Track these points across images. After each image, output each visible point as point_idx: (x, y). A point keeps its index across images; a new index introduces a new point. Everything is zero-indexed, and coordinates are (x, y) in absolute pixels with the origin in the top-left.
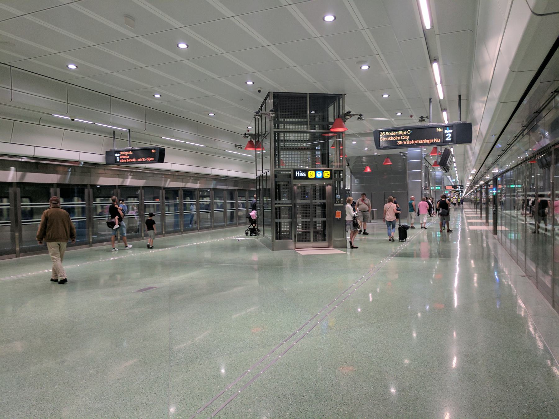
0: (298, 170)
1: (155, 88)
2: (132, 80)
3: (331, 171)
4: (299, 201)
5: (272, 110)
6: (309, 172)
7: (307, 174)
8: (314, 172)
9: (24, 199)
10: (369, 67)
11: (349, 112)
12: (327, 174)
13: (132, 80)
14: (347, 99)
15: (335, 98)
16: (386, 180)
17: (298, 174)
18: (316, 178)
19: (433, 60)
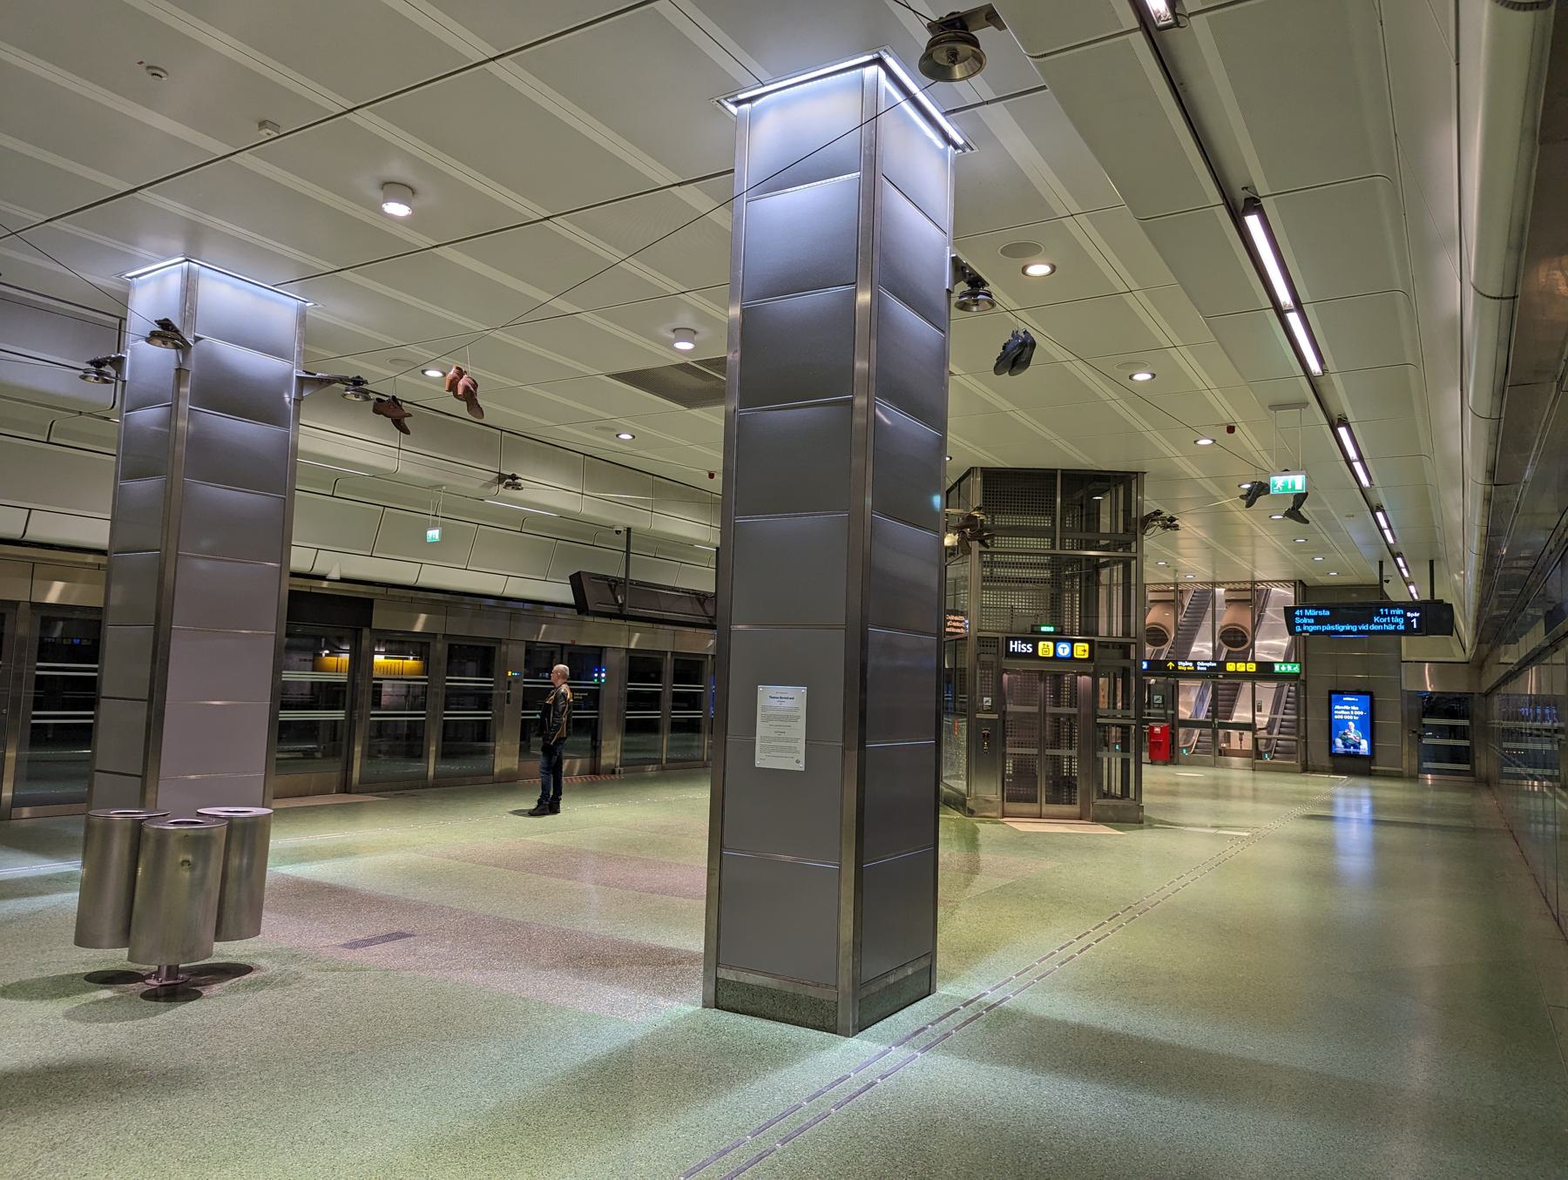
0: (1014, 639)
1: (623, 421)
2: (580, 406)
3: (1090, 642)
4: (1050, 710)
5: (979, 509)
6: (1041, 644)
7: (1035, 648)
8: (1051, 644)
9: (296, 658)
10: (1054, 268)
11: (1158, 513)
12: (1081, 650)
13: (580, 406)
14: (1148, 484)
15: (1124, 481)
16: (367, 392)
17: (1015, 646)
18: (1055, 658)
19: (1240, 206)
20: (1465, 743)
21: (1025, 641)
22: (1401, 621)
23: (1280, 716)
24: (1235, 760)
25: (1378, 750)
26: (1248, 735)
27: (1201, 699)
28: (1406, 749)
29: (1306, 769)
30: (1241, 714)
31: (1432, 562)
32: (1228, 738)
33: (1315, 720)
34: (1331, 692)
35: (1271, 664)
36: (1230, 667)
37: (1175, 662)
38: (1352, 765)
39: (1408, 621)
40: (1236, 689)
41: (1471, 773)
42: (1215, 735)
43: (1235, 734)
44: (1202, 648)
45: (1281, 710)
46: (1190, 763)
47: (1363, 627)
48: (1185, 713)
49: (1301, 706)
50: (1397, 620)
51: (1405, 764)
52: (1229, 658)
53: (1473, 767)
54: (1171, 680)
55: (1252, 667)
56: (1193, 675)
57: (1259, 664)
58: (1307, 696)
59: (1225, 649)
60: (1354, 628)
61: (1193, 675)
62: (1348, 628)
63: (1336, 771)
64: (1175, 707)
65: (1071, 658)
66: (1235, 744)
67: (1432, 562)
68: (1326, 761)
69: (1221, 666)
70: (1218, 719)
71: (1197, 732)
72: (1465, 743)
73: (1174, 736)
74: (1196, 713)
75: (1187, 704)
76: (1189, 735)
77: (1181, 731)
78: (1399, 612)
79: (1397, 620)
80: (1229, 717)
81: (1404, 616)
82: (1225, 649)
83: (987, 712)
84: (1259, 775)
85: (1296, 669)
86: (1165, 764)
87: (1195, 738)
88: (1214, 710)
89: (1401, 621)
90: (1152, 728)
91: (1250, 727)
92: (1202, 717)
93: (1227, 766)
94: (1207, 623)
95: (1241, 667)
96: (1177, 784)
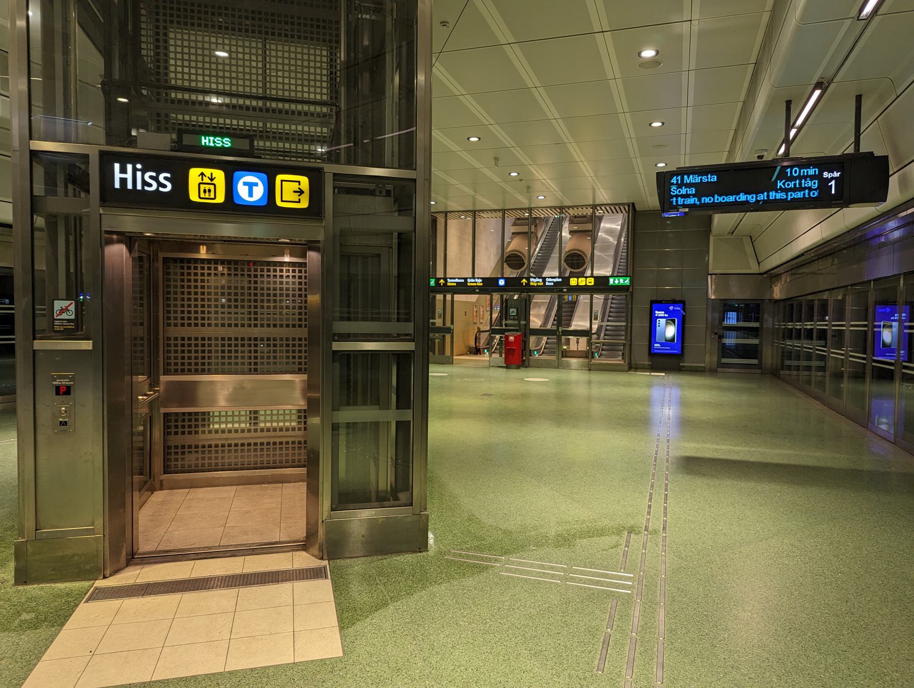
0: (124, 159)
6: (194, 174)
7: (181, 183)
12: (292, 190)
18: (232, 207)
20: (755, 341)
21: (153, 163)
22: (814, 184)
23: (605, 324)
24: (574, 361)
25: (686, 350)
26: (583, 340)
27: (549, 310)
28: (708, 346)
29: (632, 367)
30: (580, 322)
31: (859, 98)
32: (568, 342)
33: (640, 325)
34: (652, 302)
35: (606, 279)
36: (573, 282)
37: (528, 279)
38: (668, 360)
39: (824, 183)
40: (573, 305)
41: (759, 366)
42: (559, 340)
43: (573, 339)
44: (552, 273)
45: (606, 319)
46: (540, 365)
47: (761, 197)
48: (536, 322)
49: (626, 313)
50: (810, 183)
51: (707, 359)
52: (572, 275)
53: (760, 362)
54: (524, 295)
55: (591, 282)
56: (543, 289)
57: (597, 279)
58: (630, 306)
59: (569, 270)
60: (751, 198)
61: (543, 289)
62: (742, 197)
63: (654, 368)
64: (527, 319)
65: (268, 209)
66: (573, 347)
67: (859, 98)
68: (646, 362)
69: (566, 281)
70: (560, 328)
71: (545, 338)
72: (755, 341)
73: (526, 343)
74: (546, 322)
75: (537, 316)
76: (538, 343)
77: (533, 339)
78: (811, 172)
79: (810, 183)
80: (569, 325)
81: (819, 177)
82: (569, 270)
83: (68, 335)
84: (596, 377)
85: (627, 281)
86: (518, 368)
87: (544, 342)
88: (559, 320)
89: (814, 184)
90: (507, 337)
91: (586, 333)
92: (549, 327)
93: (568, 367)
94: (555, 255)
95: (582, 282)
96: (525, 396)
